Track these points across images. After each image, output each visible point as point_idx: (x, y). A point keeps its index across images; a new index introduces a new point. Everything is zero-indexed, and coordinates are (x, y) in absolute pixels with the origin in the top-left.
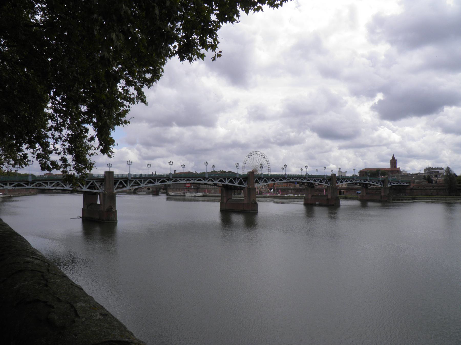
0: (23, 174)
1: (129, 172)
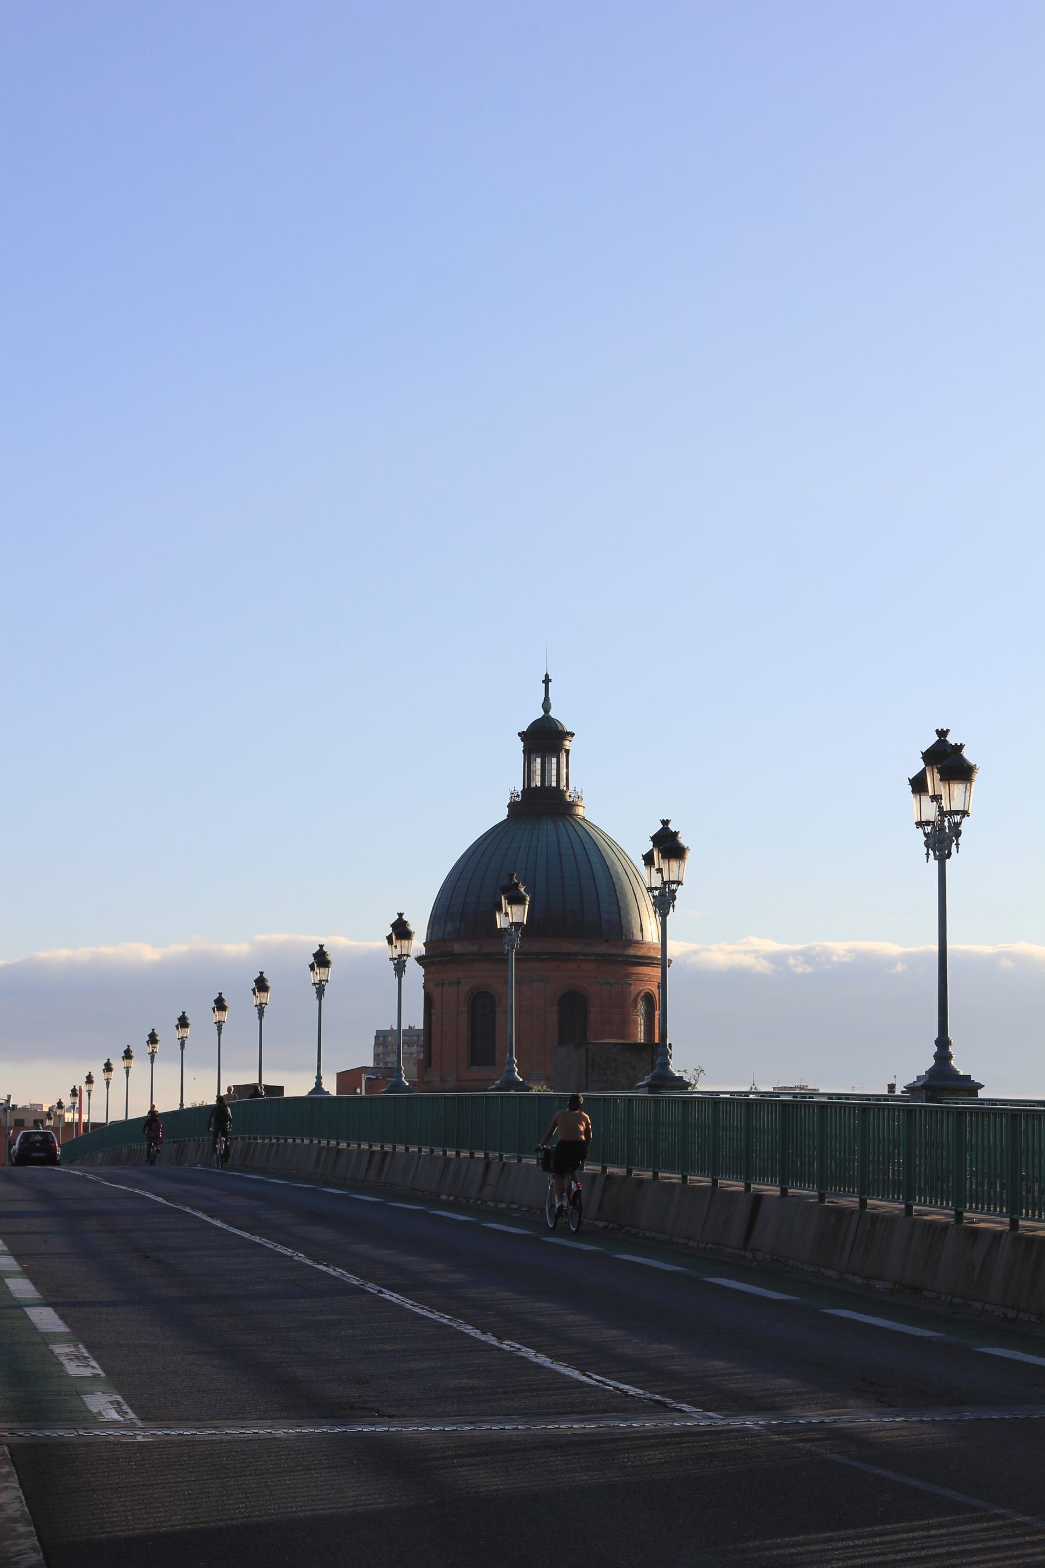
1: (546, 706)
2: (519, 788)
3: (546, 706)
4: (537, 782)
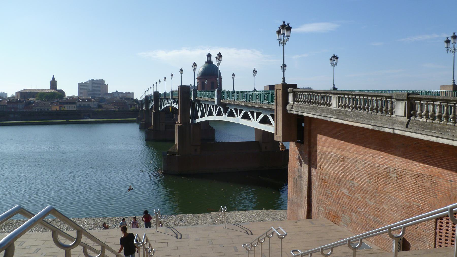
0: (96, 80)
1: (209, 52)
3: (209, 52)
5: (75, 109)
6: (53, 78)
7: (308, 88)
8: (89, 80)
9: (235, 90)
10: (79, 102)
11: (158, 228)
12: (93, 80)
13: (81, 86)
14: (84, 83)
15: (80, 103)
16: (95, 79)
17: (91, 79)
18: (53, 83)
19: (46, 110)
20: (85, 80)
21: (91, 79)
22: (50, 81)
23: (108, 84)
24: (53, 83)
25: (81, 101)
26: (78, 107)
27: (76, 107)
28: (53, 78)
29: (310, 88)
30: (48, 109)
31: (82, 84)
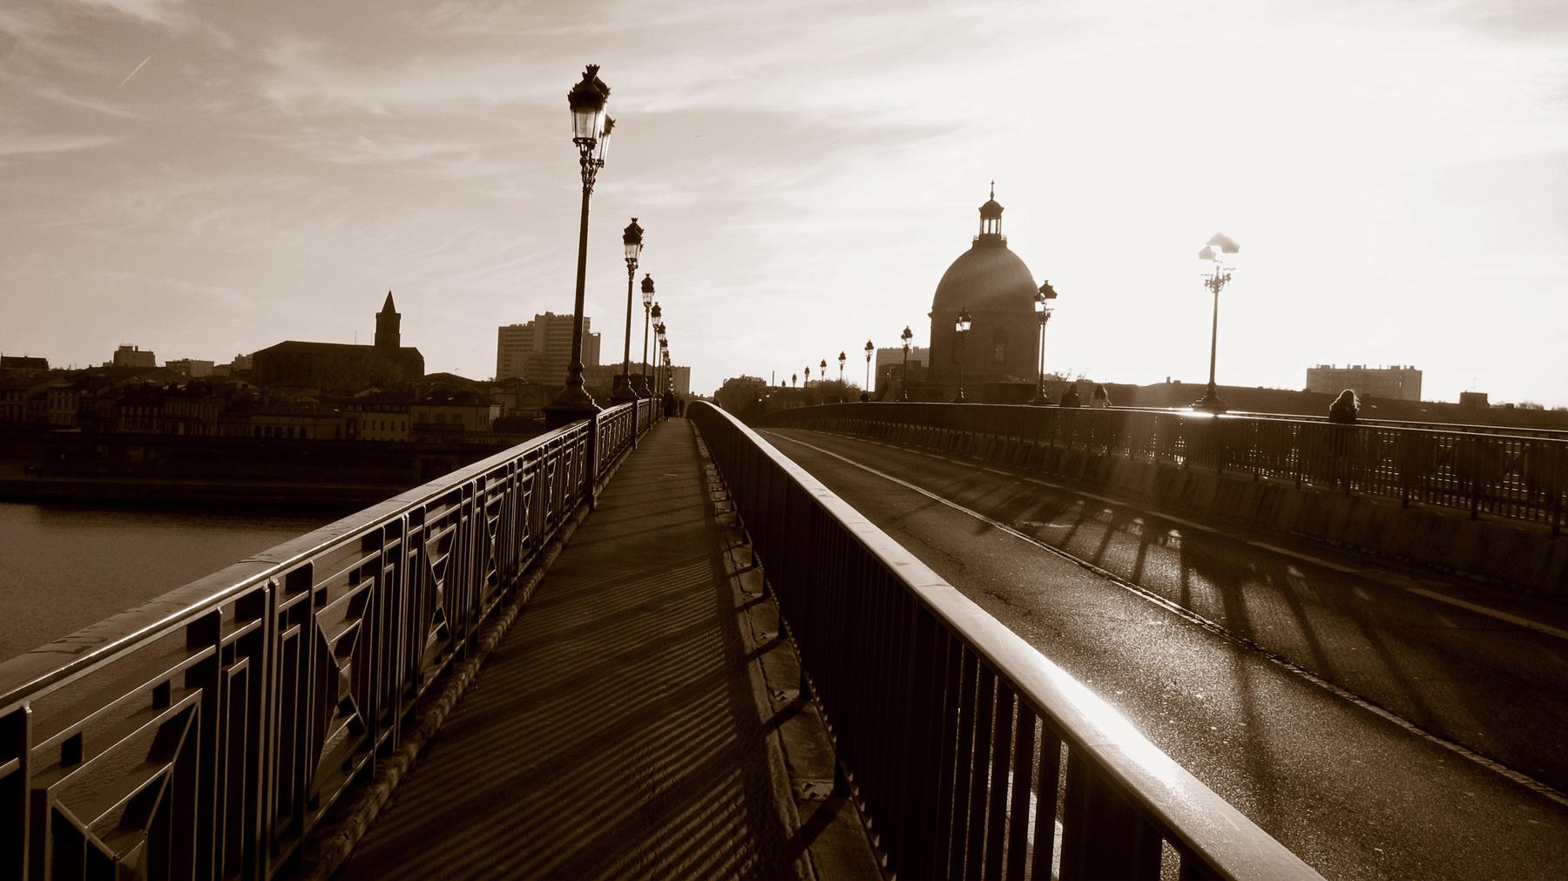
1: (992, 195)
2: (978, 235)
3: (992, 195)
4: (986, 232)
5: (398, 436)
6: (389, 302)
7: (1402, 368)
8: (537, 316)
9: (1219, 382)
10: (423, 402)
11: (1043, 310)
12: (549, 315)
13: (510, 338)
14: (520, 325)
15: (425, 409)
16: (556, 314)
17: (542, 313)
18: (388, 320)
19: (297, 434)
20: (524, 317)
21: (543, 314)
22: (378, 315)
23: (599, 334)
24: (388, 320)
25: (429, 398)
26: (414, 424)
27: (407, 428)
28: (389, 302)
29: (1412, 367)
30: (303, 432)
31: (513, 329)
